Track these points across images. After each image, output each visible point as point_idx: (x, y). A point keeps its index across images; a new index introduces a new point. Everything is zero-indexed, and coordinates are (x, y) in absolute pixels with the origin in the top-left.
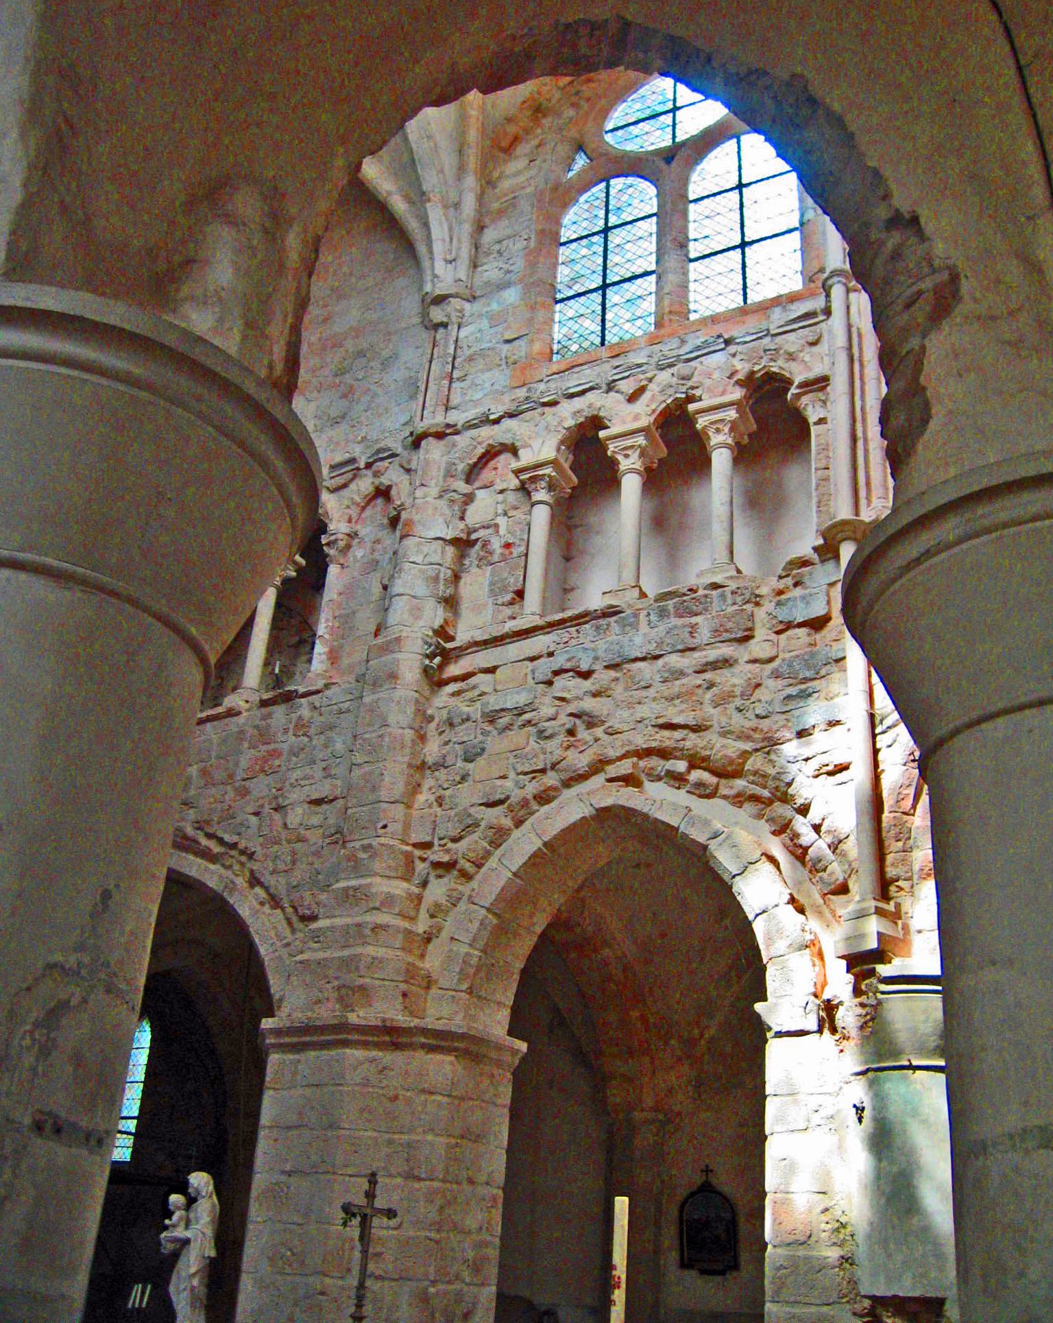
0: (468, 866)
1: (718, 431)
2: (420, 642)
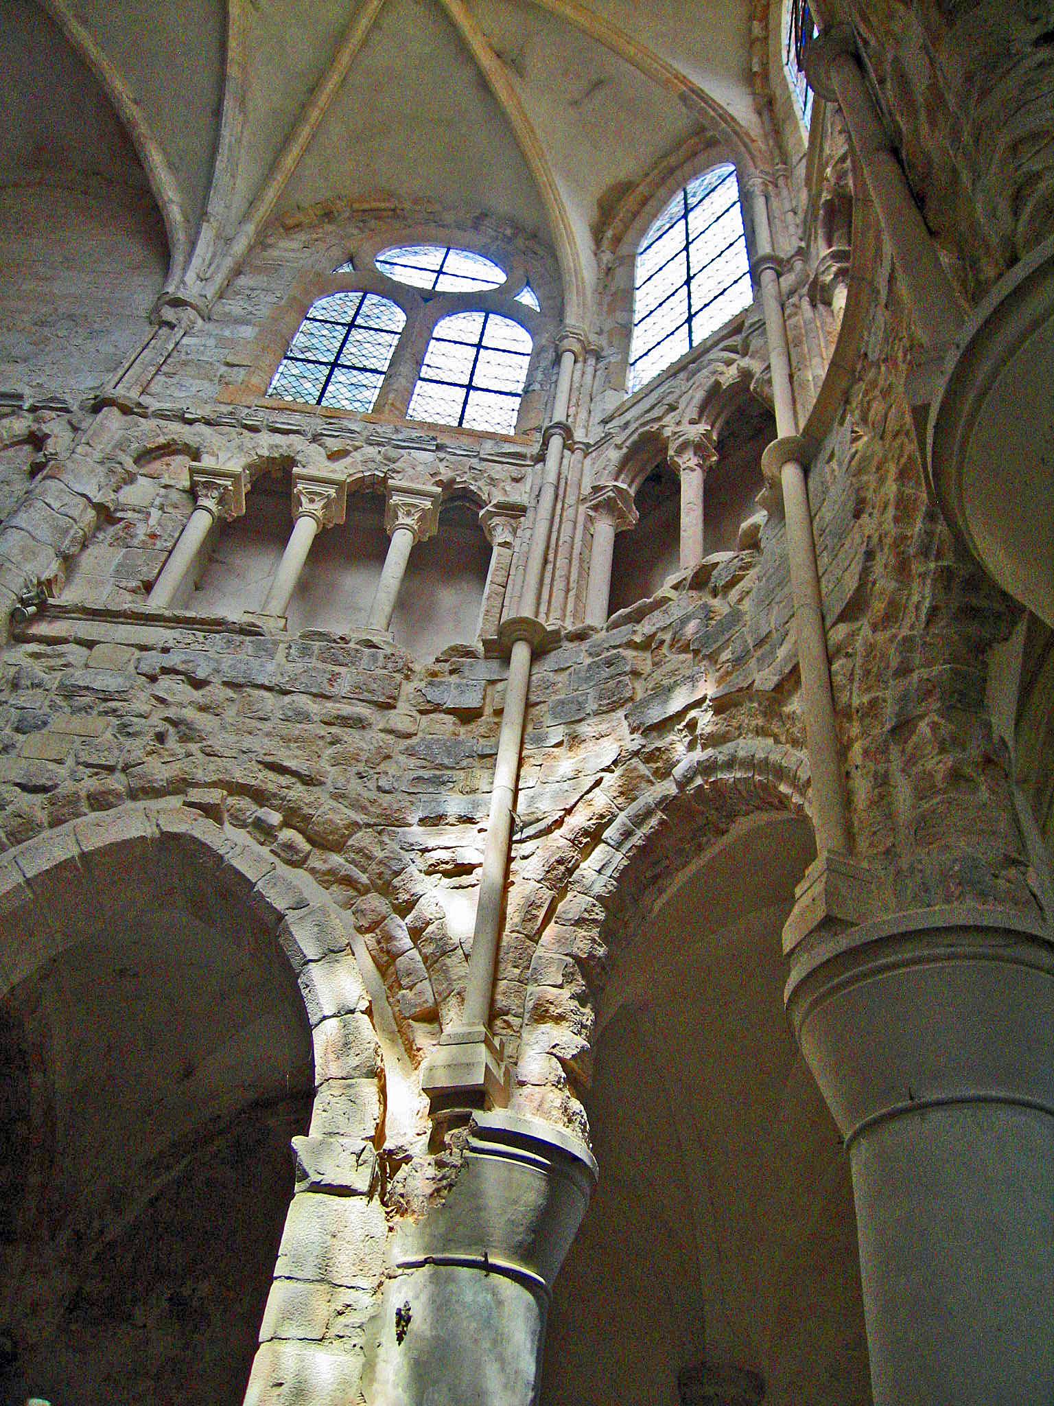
1: (408, 514)
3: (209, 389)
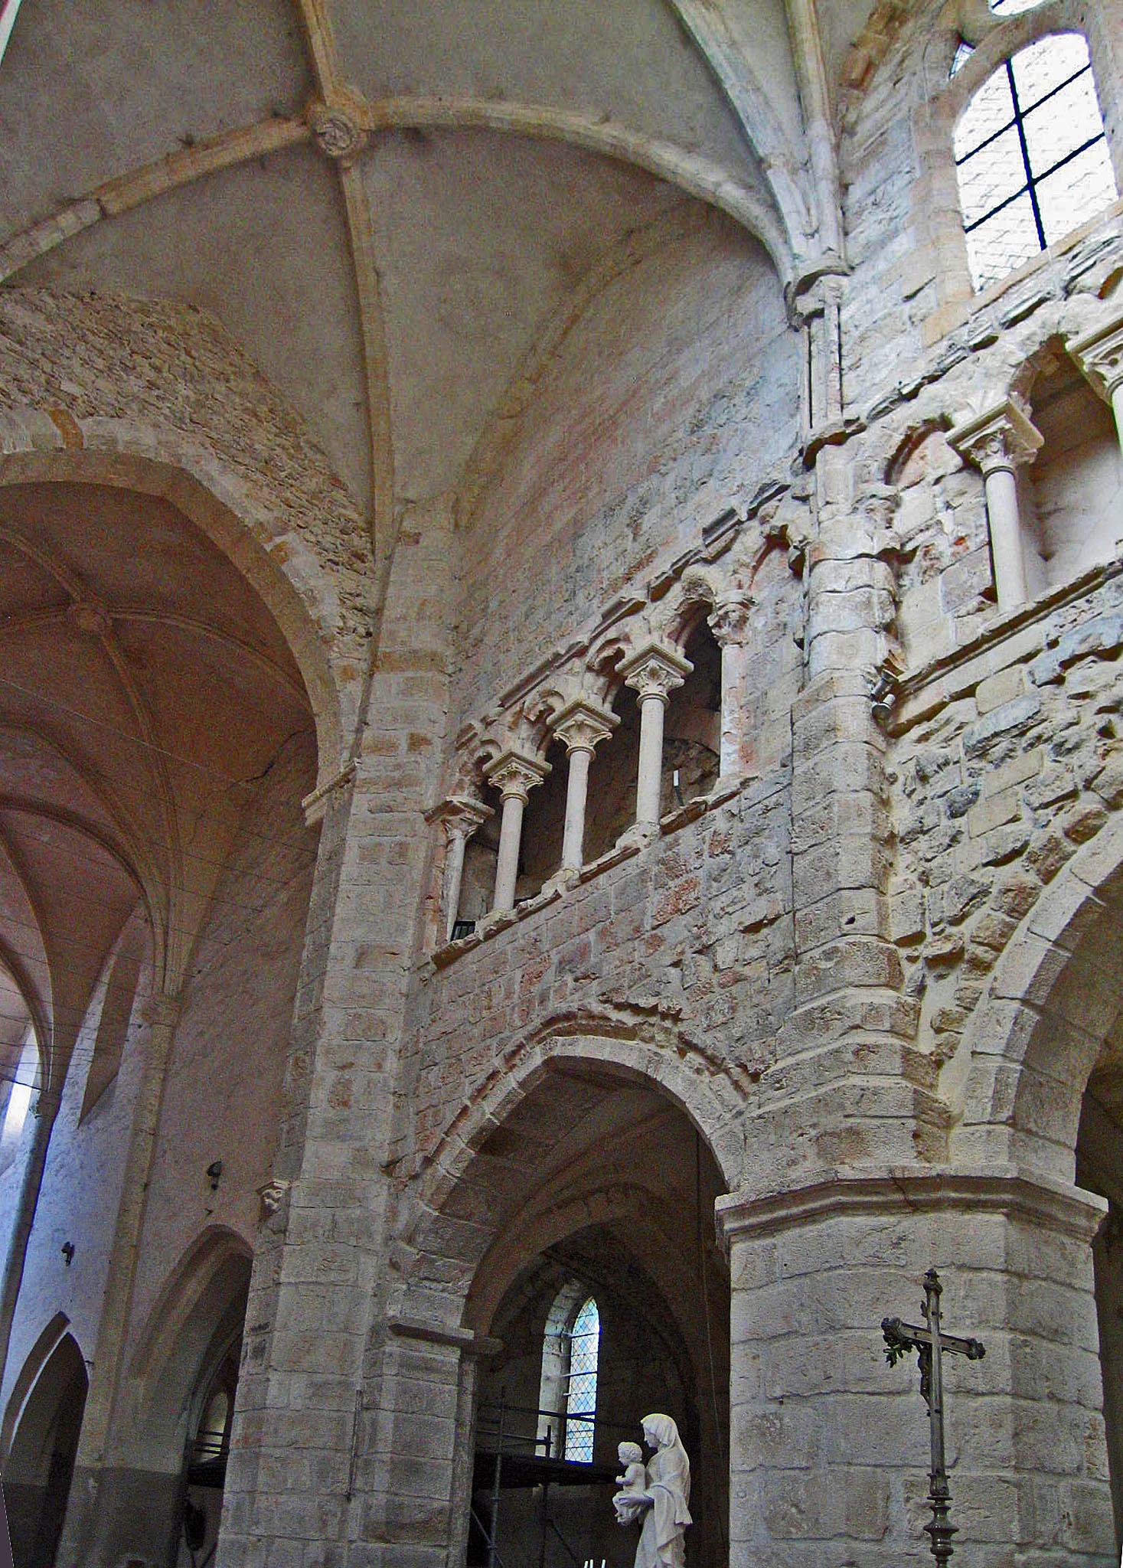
0: (980, 951)
2: (860, 681)
3: (907, 342)
